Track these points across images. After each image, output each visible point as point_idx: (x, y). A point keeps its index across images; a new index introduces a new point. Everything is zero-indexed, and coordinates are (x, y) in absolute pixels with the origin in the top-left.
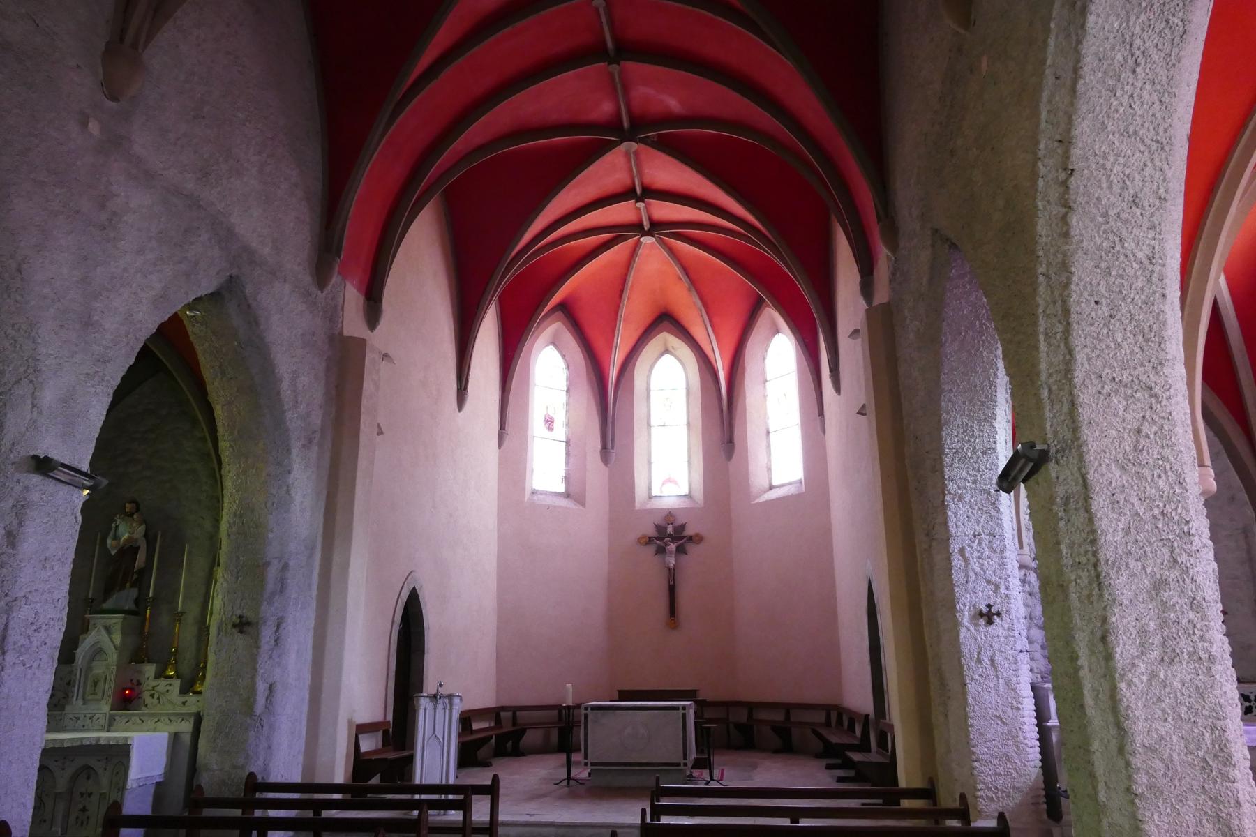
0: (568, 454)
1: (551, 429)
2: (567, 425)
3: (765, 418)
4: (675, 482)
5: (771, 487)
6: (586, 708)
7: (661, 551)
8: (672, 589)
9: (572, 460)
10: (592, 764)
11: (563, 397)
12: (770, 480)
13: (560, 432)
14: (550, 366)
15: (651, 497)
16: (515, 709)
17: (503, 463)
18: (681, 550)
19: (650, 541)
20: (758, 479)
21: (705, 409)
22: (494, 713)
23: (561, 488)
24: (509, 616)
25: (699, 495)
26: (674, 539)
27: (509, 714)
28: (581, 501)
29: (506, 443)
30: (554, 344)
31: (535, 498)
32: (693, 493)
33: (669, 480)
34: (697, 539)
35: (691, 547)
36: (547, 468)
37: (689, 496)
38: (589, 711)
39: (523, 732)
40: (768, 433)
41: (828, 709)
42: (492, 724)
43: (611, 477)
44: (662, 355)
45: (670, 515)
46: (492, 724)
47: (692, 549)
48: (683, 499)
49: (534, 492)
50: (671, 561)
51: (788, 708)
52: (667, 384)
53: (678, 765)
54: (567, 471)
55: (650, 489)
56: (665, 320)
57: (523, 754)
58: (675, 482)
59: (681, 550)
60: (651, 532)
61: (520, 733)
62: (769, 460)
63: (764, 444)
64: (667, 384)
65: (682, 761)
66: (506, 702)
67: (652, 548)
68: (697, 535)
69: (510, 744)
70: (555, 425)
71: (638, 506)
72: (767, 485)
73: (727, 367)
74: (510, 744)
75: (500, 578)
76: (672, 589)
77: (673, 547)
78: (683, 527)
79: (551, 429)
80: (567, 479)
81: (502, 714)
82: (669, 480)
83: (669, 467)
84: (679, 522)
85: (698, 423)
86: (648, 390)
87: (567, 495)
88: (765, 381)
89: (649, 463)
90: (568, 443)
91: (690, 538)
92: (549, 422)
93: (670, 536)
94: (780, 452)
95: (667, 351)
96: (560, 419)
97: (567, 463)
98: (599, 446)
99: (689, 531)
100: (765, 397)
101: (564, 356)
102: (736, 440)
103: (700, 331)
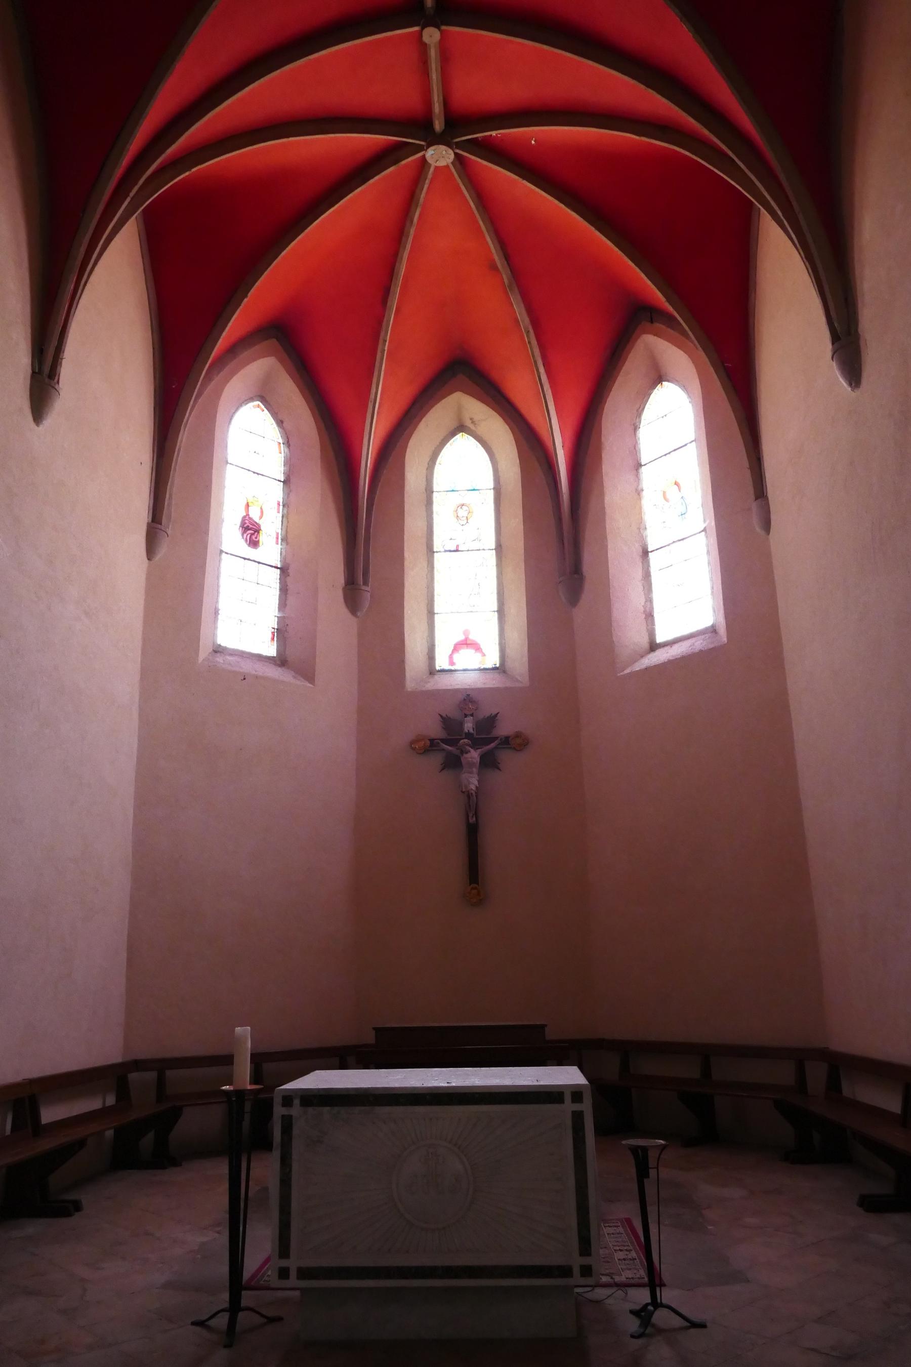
0: (284, 590)
1: (254, 543)
2: (285, 540)
3: (640, 527)
4: (476, 647)
5: (654, 647)
6: (288, 1099)
7: (453, 763)
8: (473, 832)
9: (291, 600)
10: (304, 1273)
11: (277, 492)
12: (652, 634)
13: (271, 550)
14: (253, 449)
15: (432, 672)
16: (162, 1066)
17: (155, 587)
18: (489, 762)
19: (431, 746)
20: (631, 635)
21: (529, 516)
22: (115, 1076)
23: (271, 650)
24: (156, 879)
25: (520, 665)
26: (476, 743)
27: (152, 1076)
28: (306, 672)
29: (163, 551)
30: (263, 399)
31: (220, 659)
32: (509, 664)
33: (466, 643)
34: (517, 742)
35: (507, 758)
36: (245, 611)
37: (501, 670)
38: (296, 1110)
39: (174, 1114)
40: (645, 553)
41: (800, 1057)
42: (111, 1100)
43: (361, 635)
44: (453, 434)
45: (468, 700)
46: (111, 1100)
47: (509, 759)
48: (496, 675)
49: (218, 650)
50: (472, 781)
51: (705, 1053)
52: (463, 484)
53: (565, 1271)
54: (281, 620)
55: (431, 657)
56: (461, 370)
57: (174, 1162)
58: (476, 647)
59: (489, 762)
60: (435, 730)
61: (167, 1119)
62: (649, 600)
63: (639, 573)
64: (463, 484)
65: (577, 1261)
66: (145, 1052)
67: (435, 760)
68: (518, 735)
69: (148, 1140)
70: (262, 538)
71: (410, 685)
72: (644, 641)
73: (570, 433)
74: (148, 1140)
75: (142, 801)
76: (473, 832)
77: (474, 755)
78: (492, 720)
79: (254, 544)
80: (281, 633)
81: (133, 1076)
82: (466, 643)
83: (465, 614)
84: (486, 711)
85: (517, 544)
86: (429, 491)
87: (281, 661)
88: (639, 465)
89: (431, 613)
90: (284, 570)
91: (506, 742)
92: (251, 531)
93: (469, 735)
94: (674, 583)
95: (461, 428)
96: (271, 525)
97: (282, 605)
98: (341, 580)
99: (504, 729)
100: (639, 492)
101: (280, 423)
102: (586, 569)
103: (518, 386)
